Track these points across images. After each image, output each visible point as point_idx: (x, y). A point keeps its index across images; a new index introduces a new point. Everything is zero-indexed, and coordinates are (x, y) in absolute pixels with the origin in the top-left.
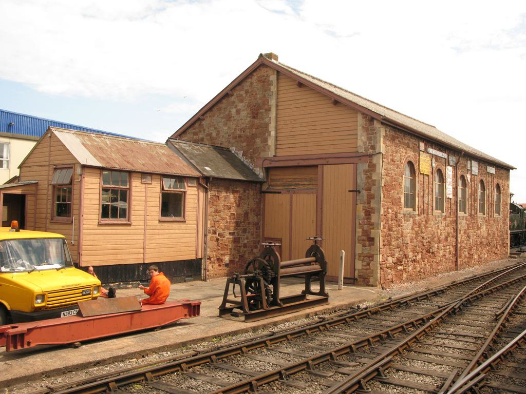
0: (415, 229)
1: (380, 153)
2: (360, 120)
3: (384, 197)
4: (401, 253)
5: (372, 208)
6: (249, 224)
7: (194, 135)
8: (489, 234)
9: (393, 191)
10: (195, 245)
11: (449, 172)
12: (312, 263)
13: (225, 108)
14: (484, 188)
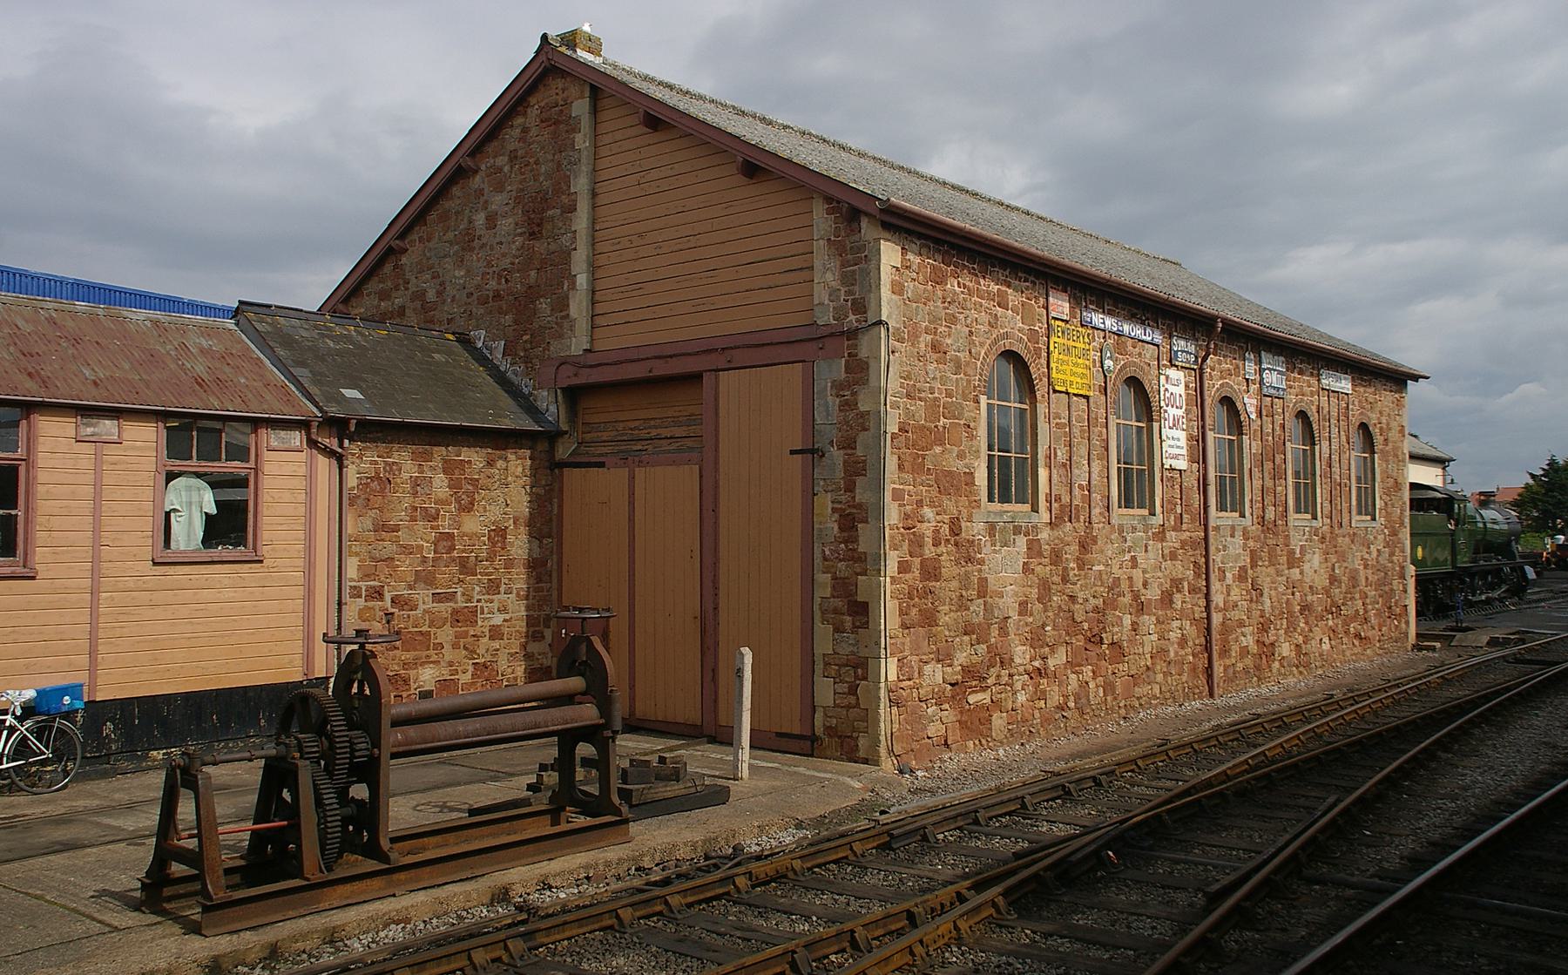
0: (1039, 569)
1: (880, 322)
2: (821, 221)
3: (901, 467)
4: (982, 648)
5: (860, 506)
6: (509, 564)
7: (381, 300)
8: (1333, 579)
9: (938, 449)
10: (300, 635)
11: (1173, 386)
12: (578, 698)
13: (457, 213)
14: (1312, 437)
